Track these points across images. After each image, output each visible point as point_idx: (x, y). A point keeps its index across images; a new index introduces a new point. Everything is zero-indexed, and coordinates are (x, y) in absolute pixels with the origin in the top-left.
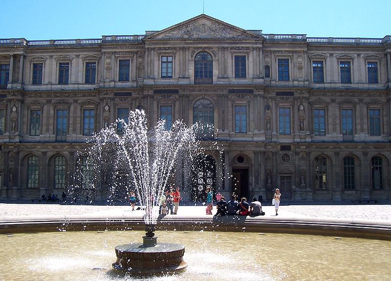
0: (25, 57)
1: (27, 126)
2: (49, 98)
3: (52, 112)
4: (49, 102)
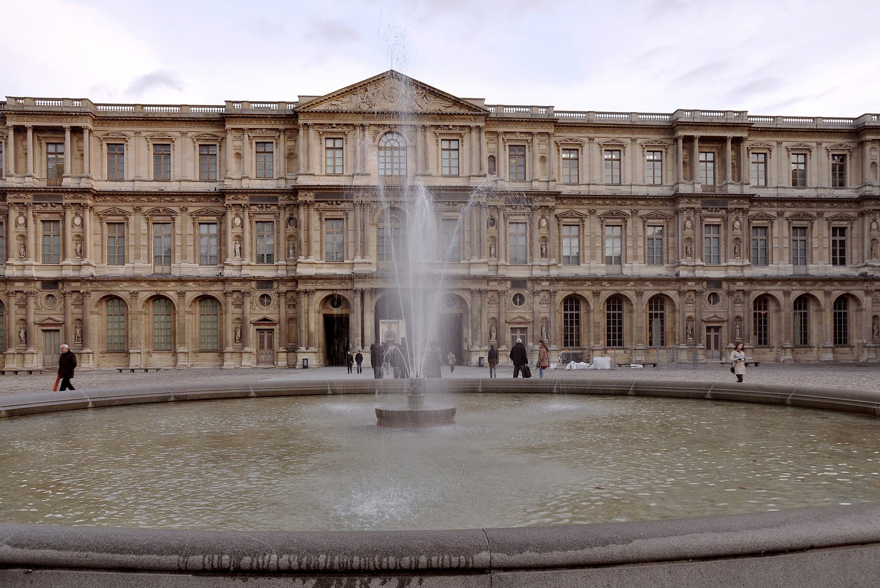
0: (90, 131)
1: (102, 249)
2: (139, 204)
3: (144, 226)
4: (137, 210)
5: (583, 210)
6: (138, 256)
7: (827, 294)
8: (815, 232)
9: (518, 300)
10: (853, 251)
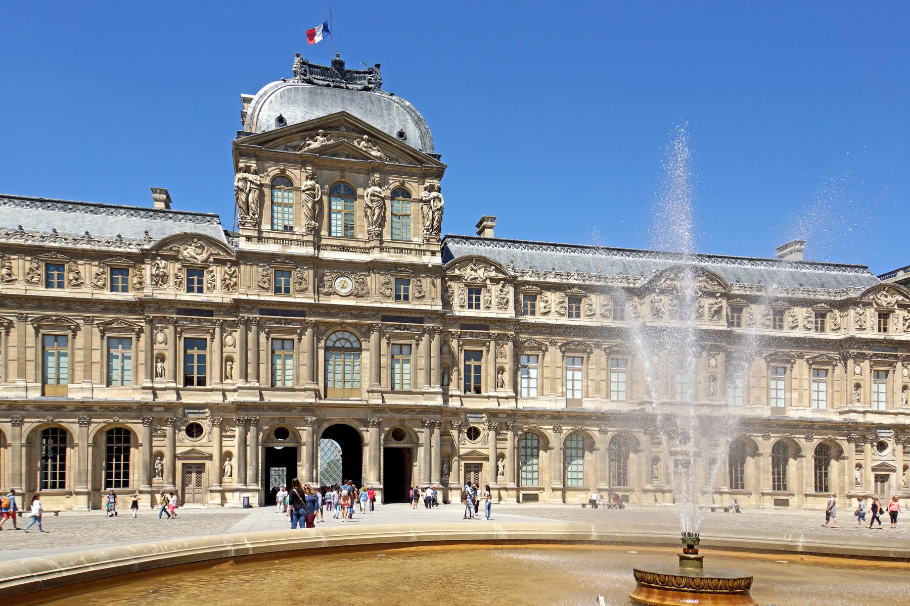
7: (557, 431)
9: (473, 434)
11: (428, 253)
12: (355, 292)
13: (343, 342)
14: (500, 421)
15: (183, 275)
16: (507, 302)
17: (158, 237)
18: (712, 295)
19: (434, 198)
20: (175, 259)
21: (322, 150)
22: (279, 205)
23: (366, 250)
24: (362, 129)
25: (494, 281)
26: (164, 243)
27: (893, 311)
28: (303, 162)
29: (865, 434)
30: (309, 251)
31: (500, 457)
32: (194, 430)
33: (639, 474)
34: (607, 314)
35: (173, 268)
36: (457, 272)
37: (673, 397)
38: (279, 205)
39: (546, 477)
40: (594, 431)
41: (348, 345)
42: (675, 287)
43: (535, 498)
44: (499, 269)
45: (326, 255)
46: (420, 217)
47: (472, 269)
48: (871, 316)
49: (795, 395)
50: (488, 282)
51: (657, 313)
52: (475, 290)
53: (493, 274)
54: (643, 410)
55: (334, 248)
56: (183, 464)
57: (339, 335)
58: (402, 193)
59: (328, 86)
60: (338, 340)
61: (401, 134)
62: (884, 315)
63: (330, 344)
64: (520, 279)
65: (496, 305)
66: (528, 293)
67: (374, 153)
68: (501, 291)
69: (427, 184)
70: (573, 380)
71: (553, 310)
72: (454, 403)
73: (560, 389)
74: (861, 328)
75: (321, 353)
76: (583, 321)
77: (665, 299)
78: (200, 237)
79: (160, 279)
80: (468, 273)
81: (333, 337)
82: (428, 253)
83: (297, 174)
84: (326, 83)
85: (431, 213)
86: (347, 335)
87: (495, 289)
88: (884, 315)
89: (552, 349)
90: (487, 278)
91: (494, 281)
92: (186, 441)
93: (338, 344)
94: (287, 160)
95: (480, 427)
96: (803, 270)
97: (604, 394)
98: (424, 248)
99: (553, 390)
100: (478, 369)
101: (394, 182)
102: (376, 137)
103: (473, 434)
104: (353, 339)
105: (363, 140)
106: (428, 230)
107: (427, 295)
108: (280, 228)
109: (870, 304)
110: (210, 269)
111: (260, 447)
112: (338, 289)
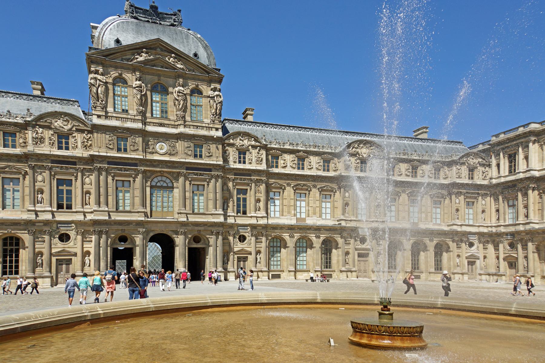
5: (310, 184)
6: (257, 209)
8: (286, 193)
9: (242, 239)
10: (476, 177)
11: (214, 129)
12: (169, 152)
13: (162, 183)
14: (258, 231)
15: (55, 138)
16: (262, 160)
17: (37, 114)
18: (82, 131)
19: (217, 96)
20: (49, 128)
21: (145, 62)
22: (119, 96)
23: (175, 126)
24: (171, 51)
25: (254, 147)
26: (41, 117)
27: (477, 168)
28: (133, 69)
29: (462, 238)
30: (139, 125)
31: (258, 252)
32: (64, 238)
33: (338, 262)
34: (320, 168)
35: (48, 134)
36: (231, 141)
37: (356, 217)
38: (119, 96)
39: (285, 264)
40: (313, 237)
41: (165, 185)
42: (358, 153)
43: (278, 276)
44: (256, 140)
45: (150, 128)
46: (209, 107)
47: (241, 140)
48: (464, 170)
49: (423, 215)
50: (250, 147)
51: (347, 168)
52: (242, 153)
53: (253, 143)
54: (340, 224)
55: (155, 124)
56: (57, 259)
57: (160, 178)
58: (196, 91)
59: (148, 21)
60: (159, 181)
61: (196, 55)
62: (472, 170)
63: (154, 184)
64: (269, 146)
65: (255, 162)
66: (273, 155)
67: (179, 66)
68: (258, 153)
69: (212, 87)
70: (300, 207)
71: (288, 165)
72: (231, 220)
73: (293, 212)
74: (459, 177)
75: (148, 189)
76: (306, 172)
77: (353, 159)
78: (66, 114)
79: (39, 141)
80: (238, 142)
81: (156, 180)
82: (214, 129)
83: (127, 76)
84: (147, 19)
85: (215, 105)
86: (164, 179)
87: (254, 152)
88: (472, 170)
89: (288, 188)
90: (249, 145)
91: (254, 147)
92: (59, 244)
93: (159, 184)
94: (123, 67)
95: (246, 235)
96: (428, 144)
97: (318, 215)
98: (211, 126)
99: (289, 212)
100: (245, 200)
101: (192, 85)
102: (180, 56)
103: (242, 239)
104: (168, 181)
105: (171, 57)
106: (213, 115)
107: (214, 155)
108: (120, 111)
109: (463, 164)
110: (74, 135)
111: (109, 248)
112: (158, 150)
